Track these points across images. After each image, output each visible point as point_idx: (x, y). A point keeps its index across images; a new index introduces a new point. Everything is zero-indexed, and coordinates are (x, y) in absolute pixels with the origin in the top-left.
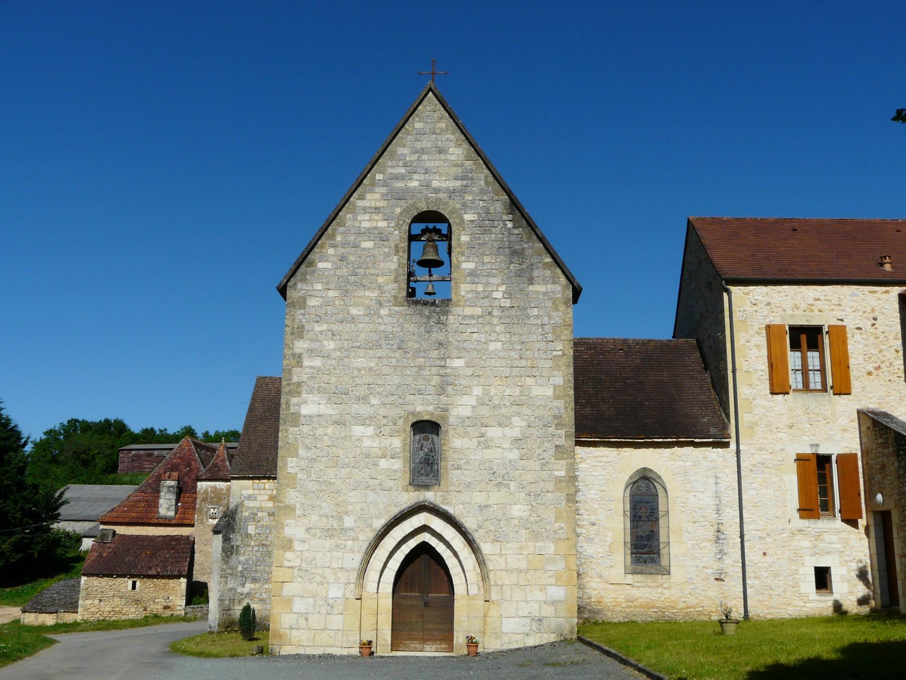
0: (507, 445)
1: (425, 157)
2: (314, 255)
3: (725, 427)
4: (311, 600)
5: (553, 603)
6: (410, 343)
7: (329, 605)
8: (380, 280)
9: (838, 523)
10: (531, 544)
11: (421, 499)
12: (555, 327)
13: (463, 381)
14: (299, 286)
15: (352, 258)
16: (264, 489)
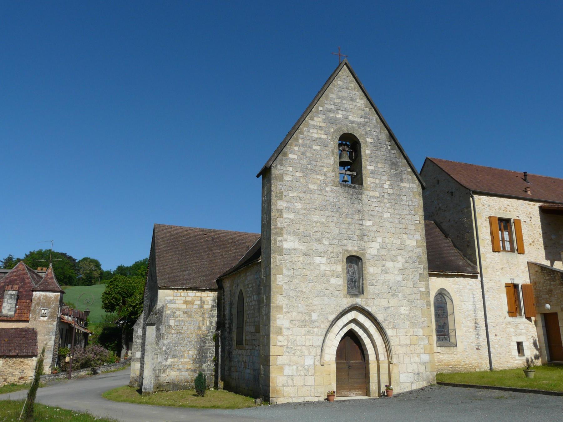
0: (396, 272)
1: (344, 102)
2: (287, 149)
3: (474, 268)
4: (295, 367)
5: (425, 363)
6: (344, 209)
7: (305, 370)
8: (325, 170)
9: (524, 319)
10: (411, 330)
11: (354, 303)
12: (415, 207)
13: (372, 234)
14: (279, 167)
15: (308, 154)
16: (181, 296)
